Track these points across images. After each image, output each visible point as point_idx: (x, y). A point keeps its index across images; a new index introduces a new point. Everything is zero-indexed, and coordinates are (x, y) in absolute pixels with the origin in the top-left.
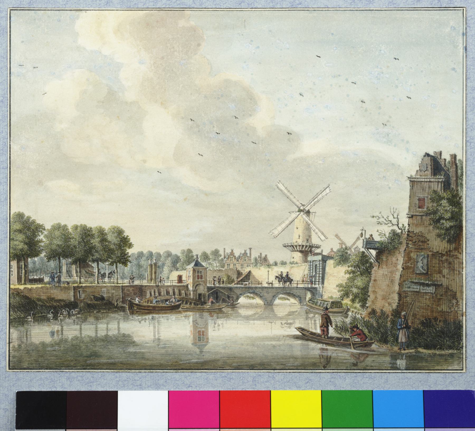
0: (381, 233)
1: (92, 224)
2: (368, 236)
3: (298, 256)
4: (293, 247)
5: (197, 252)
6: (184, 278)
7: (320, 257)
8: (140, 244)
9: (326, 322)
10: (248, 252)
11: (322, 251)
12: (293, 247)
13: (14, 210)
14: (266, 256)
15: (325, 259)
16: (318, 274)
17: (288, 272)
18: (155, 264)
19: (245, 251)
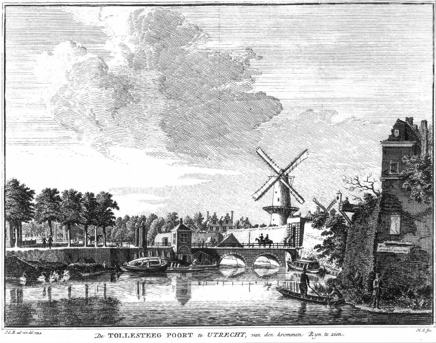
0: (356, 197)
1: (82, 189)
2: (344, 199)
3: (277, 218)
4: (270, 209)
5: (182, 215)
6: (169, 241)
7: (298, 220)
8: (127, 208)
9: (305, 279)
10: (230, 215)
11: (300, 214)
12: (270, 209)
13: (9, 178)
14: (215, 214)
15: (304, 221)
16: (295, 237)
17: (267, 235)
18: (142, 226)
19: (228, 214)
